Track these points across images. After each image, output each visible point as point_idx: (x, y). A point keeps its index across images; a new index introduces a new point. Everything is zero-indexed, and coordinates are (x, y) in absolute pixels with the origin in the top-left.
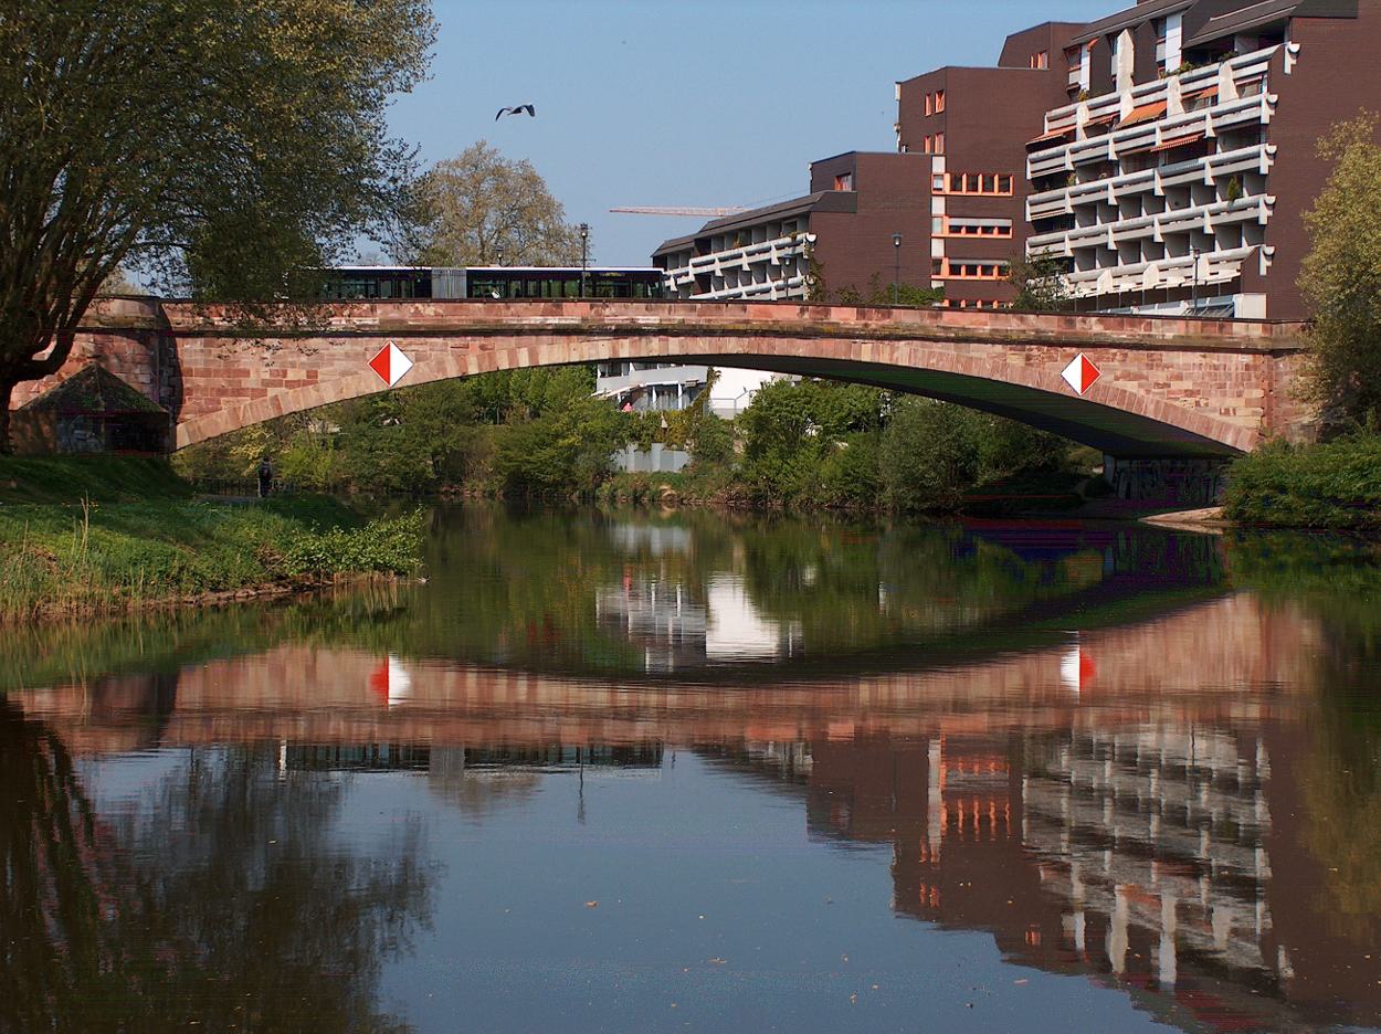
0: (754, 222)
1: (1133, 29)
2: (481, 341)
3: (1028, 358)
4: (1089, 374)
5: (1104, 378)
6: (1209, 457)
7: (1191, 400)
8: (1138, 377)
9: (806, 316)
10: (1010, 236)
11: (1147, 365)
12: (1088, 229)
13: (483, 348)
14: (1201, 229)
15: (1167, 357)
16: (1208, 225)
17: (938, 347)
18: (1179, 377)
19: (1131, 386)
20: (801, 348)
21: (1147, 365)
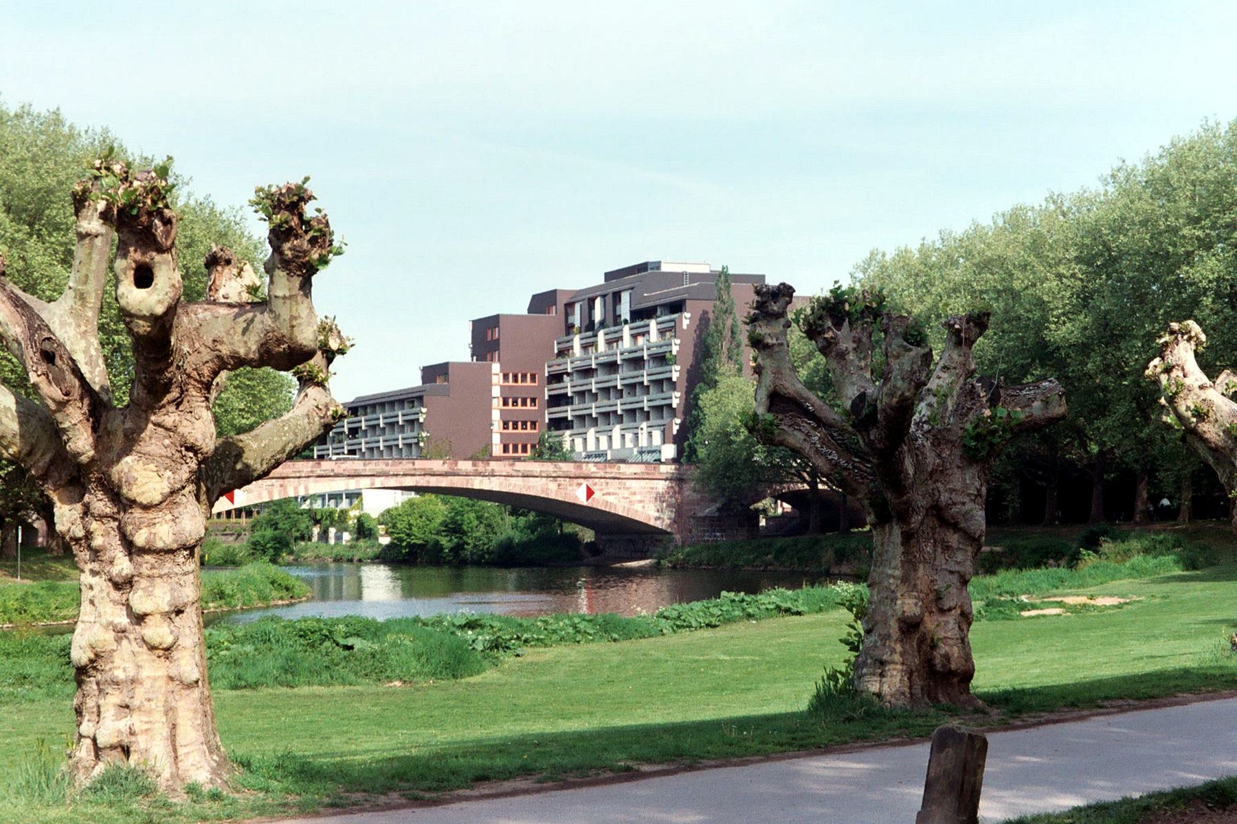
0: (387, 399)
1: (604, 296)
2: (281, 481)
3: (559, 485)
4: (590, 493)
5: (597, 495)
6: (652, 533)
7: (641, 505)
8: (614, 494)
9: (446, 466)
10: (536, 408)
11: (222, 343)
12: (581, 406)
13: (281, 486)
14: (642, 383)
15: (629, 483)
16: (646, 406)
17: (512, 480)
18: (634, 494)
19: (610, 499)
20: (444, 482)
21: (222, 343)
